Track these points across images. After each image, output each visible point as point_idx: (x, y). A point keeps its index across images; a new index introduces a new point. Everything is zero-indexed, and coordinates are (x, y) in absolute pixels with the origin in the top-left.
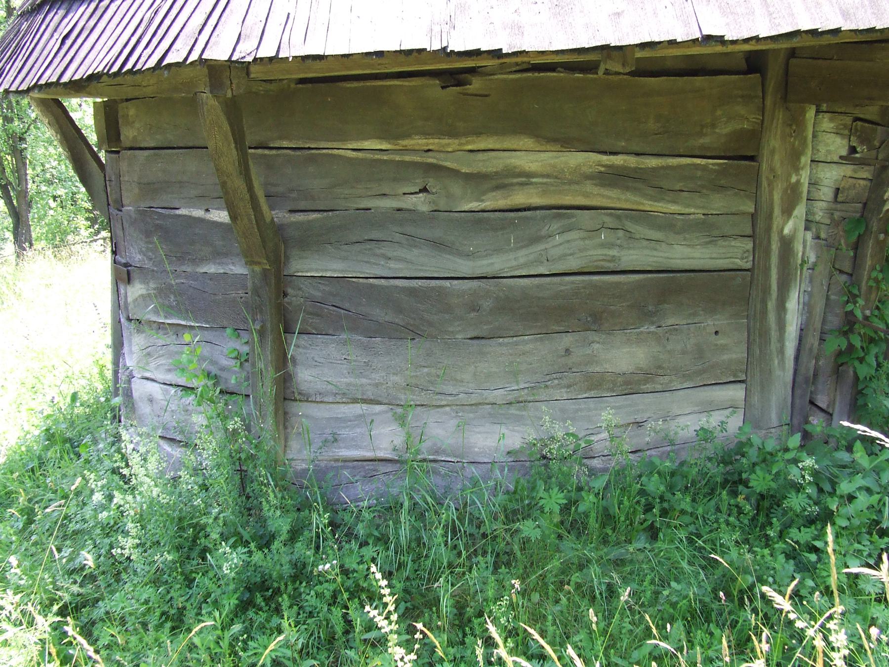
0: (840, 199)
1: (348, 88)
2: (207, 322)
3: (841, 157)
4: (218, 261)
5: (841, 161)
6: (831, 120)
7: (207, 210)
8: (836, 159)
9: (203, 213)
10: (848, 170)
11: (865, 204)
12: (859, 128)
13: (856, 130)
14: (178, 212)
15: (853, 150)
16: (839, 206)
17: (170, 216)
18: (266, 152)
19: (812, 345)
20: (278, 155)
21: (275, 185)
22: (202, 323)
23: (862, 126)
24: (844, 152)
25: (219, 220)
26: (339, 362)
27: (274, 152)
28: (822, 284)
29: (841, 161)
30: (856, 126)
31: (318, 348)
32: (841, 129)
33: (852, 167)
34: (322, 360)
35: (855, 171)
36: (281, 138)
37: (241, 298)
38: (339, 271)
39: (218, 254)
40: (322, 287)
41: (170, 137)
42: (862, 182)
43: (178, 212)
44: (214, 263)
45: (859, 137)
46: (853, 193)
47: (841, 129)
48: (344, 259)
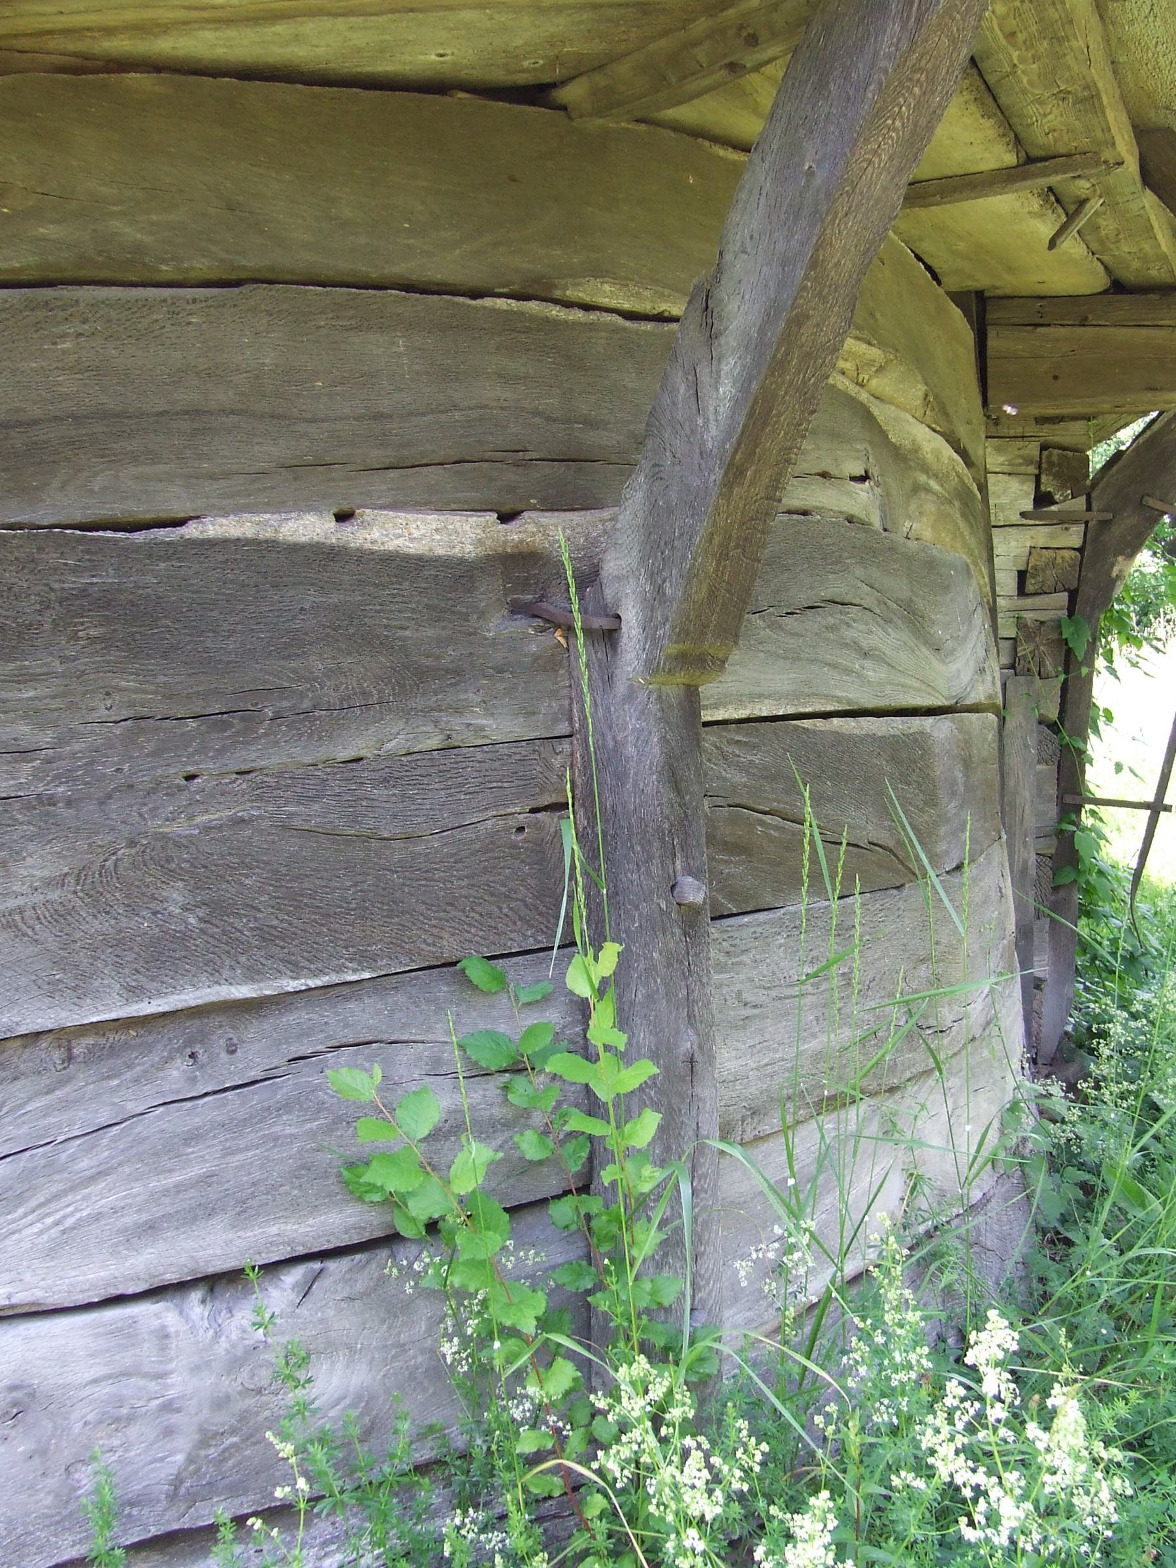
0: (1030, 587)
1: (721, 158)
2: (365, 958)
3: (1023, 515)
4: (419, 702)
5: (1025, 521)
6: (998, 450)
7: (343, 517)
8: (1015, 518)
9: (332, 524)
10: (1041, 535)
11: (1073, 595)
12: (1055, 459)
13: (1051, 464)
14: (191, 531)
15: (1042, 499)
16: (1029, 602)
17: (153, 552)
18: (555, 312)
19: (1025, 862)
20: (591, 326)
21: (590, 423)
22: (339, 970)
23: (1061, 457)
24: (1028, 505)
25: (413, 548)
26: (795, 991)
27: (578, 315)
28: (1026, 746)
29: (1025, 521)
30: (1049, 456)
31: (745, 958)
32: (1020, 465)
33: (1047, 529)
34: (760, 997)
35: (1052, 536)
36: (598, 272)
37: (521, 829)
38: (777, 697)
39: (422, 675)
40: (746, 757)
41: (128, 231)
42: (1066, 553)
43: (191, 531)
44: (407, 714)
45: (1057, 476)
46: (1051, 575)
47: (1020, 465)
48: (793, 658)
